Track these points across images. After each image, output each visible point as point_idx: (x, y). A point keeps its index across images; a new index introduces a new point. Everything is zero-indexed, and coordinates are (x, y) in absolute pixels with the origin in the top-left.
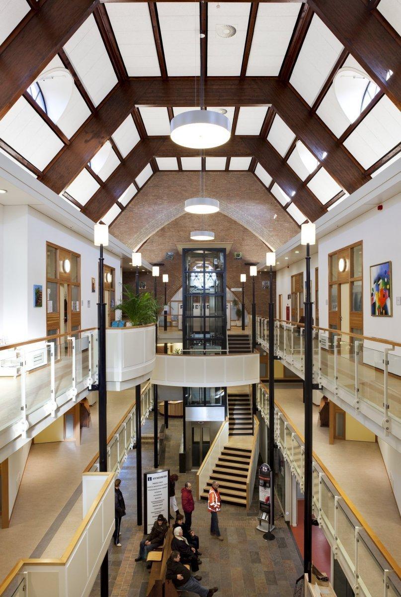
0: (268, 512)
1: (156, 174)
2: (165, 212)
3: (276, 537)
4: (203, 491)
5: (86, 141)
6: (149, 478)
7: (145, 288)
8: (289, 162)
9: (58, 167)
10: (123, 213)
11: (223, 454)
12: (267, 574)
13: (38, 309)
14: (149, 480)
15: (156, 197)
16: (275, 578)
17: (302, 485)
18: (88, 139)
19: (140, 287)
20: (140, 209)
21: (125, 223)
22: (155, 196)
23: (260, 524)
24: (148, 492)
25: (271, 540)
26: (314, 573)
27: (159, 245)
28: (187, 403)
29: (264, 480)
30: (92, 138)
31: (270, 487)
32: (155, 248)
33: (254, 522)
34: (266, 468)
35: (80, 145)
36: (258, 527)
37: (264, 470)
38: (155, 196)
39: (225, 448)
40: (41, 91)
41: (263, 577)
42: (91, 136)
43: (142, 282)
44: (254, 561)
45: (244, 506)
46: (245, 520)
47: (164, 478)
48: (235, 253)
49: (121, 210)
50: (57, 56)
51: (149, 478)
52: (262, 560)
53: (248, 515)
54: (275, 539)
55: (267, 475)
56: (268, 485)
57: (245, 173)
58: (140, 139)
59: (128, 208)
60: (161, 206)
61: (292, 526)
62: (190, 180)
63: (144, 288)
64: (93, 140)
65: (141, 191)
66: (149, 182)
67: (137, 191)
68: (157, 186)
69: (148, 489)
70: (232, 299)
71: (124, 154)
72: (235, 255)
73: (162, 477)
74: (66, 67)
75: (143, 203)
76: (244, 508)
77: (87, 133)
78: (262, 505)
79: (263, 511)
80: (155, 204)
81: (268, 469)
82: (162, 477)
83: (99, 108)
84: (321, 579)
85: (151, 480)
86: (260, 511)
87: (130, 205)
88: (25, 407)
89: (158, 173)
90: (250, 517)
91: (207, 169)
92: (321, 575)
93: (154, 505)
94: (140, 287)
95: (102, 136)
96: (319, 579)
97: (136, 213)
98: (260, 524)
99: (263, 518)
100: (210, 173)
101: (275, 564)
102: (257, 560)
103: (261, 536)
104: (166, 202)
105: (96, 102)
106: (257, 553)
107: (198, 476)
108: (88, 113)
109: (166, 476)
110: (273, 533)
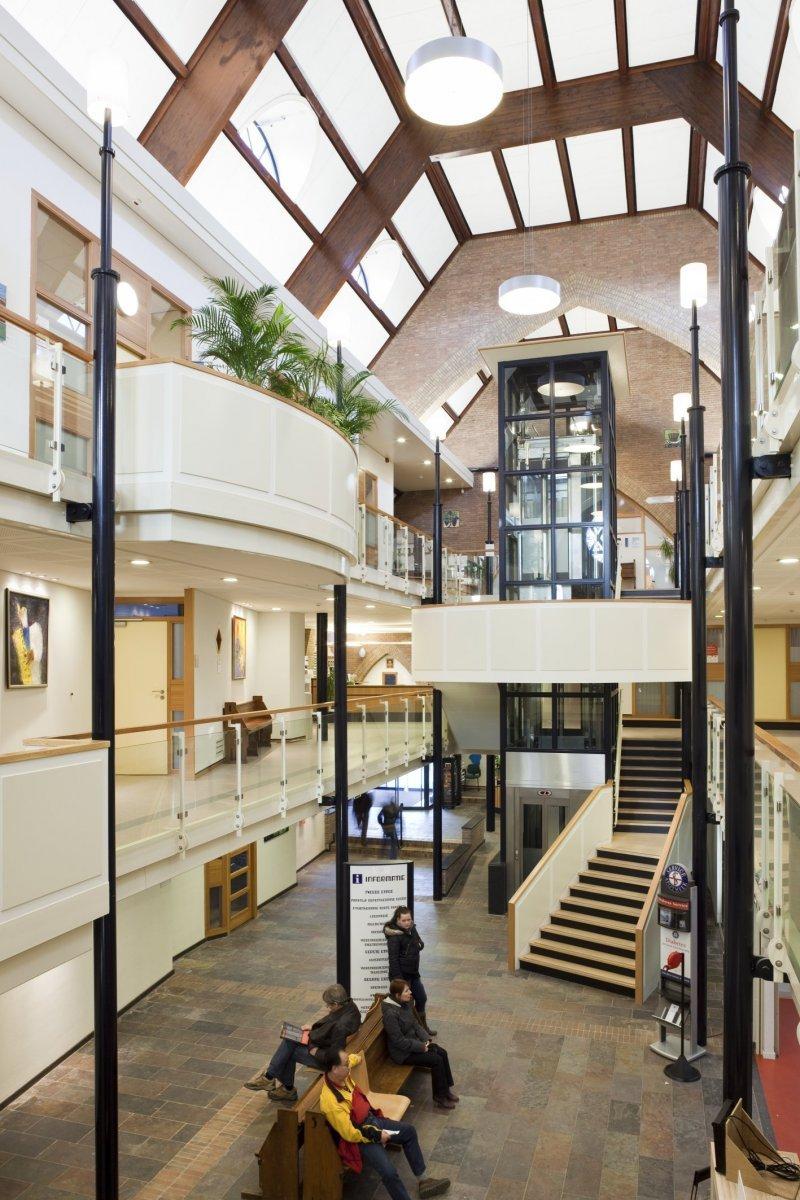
0: (684, 1006)
1: (464, 246)
2: (486, 329)
3: (703, 1075)
4: (527, 949)
5: (224, 61)
6: (354, 876)
7: (457, 525)
8: (777, 109)
9: (163, 133)
10: (393, 342)
11: (592, 866)
12: (646, 1165)
13: (577, 878)
14: (354, 882)
15: (467, 298)
16: (670, 1181)
17: (718, 803)
18: (228, 55)
19: (447, 524)
20: (433, 329)
21: (398, 364)
22: (463, 295)
23: (663, 1039)
24: (354, 914)
25: (686, 1080)
26: (743, 1144)
27: (487, 427)
28: (514, 739)
29: (673, 909)
30: (234, 53)
31: (688, 929)
32: (478, 434)
33: (649, 1033)
34: (678, 876)
35: (214, 79)
36: (656, 1046)
37: (672, 881)
38: (463, 295)
39: (601, 854)
40: (268, 146)
41: (633, 1174)
42: (232, 47)
43: (450, 513)
44: (617, 1126)
45: (628, 992)
46: (625, 1026)
47: (395, 882)
48: (667, 432)
49: (388, 336)
50: (384, 230)
51: (354, 876)
52: (643, 1127)
53: (637, 1015)
54: (700, 1081)
55: (681, 896)
56: (683, 923)
57: (679, 212)
58: (399, 121)
59: (404, 329)
60: (477, 317)
61: (761, 1056)
62: (545, 248)
63: (454, 524)
64: (239, 53)
65: (433, 289)
66: (450, 266)
67: (481, 384)
68: (468, 272)
69: (353, 904)
70: (660, 542)
71: (364, 162)
72: (667, 437)
73: (391, 878)
74: (303, 95)
75: (438, 315)
76: (629, 998)
77: (224, 40)
78: (671, 986)
79: (671, 1001)
80: (464, 312)
81: (685, 879)
82: (391, 878)
83: (369, 173)
84: (771, 1169)
85: (361, 882)
86: (661, 999)
87: (408, 322)
88: (184, 752)
89: (470, 243)
90: (639, 1021)
91: (583, 216)
92: (773, 1155)
93: (368, 948)
94: (447, 524)
95: (258, 40)
96: (759, 1166)
97: (421, 339)
98: (663, 1039)
99: (669, 1018)
100: (593, 225)
101: (681, 1145)
102: (627, 1120)
103: (659, 1069)
104: (488, 305)
105: (364, 162)
106: (634, 1108)
107: (513, 905)
108: (350, 183)
109: (401, 878)
110: (697, 1066)
